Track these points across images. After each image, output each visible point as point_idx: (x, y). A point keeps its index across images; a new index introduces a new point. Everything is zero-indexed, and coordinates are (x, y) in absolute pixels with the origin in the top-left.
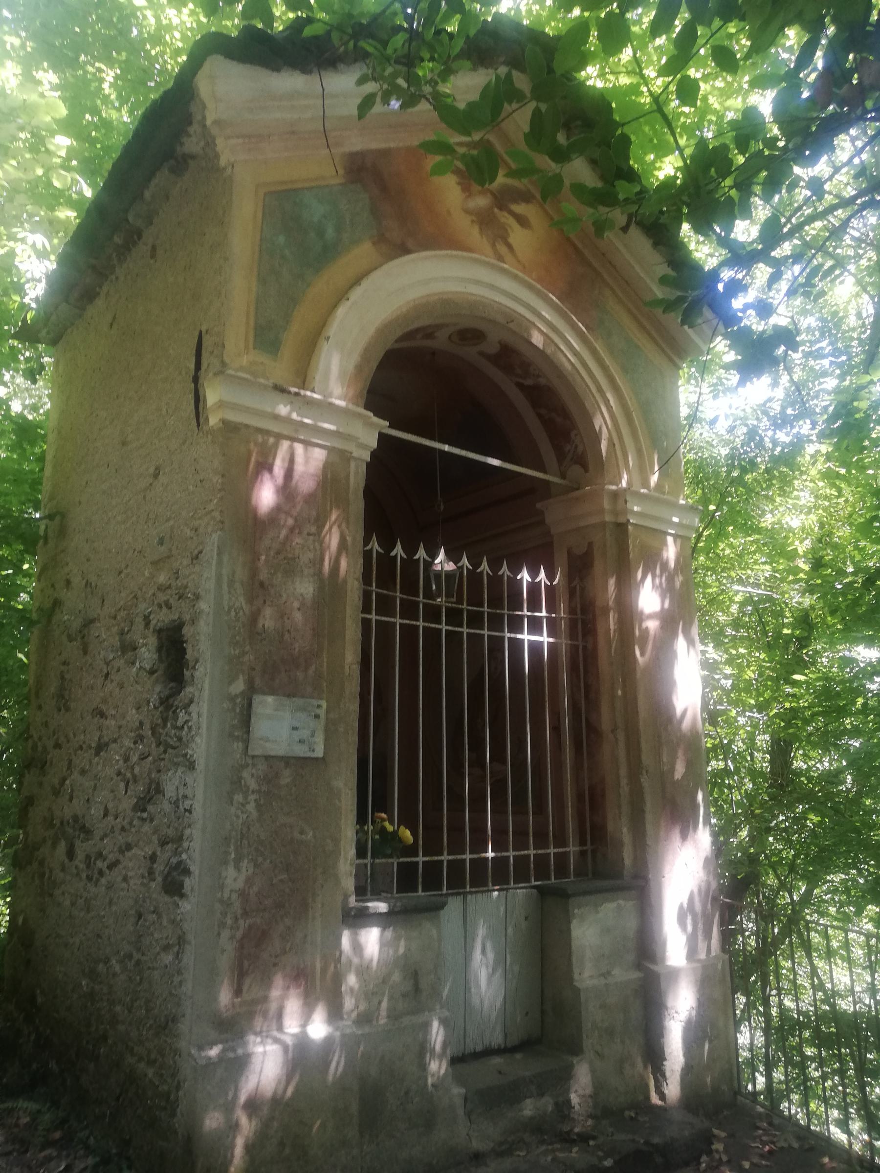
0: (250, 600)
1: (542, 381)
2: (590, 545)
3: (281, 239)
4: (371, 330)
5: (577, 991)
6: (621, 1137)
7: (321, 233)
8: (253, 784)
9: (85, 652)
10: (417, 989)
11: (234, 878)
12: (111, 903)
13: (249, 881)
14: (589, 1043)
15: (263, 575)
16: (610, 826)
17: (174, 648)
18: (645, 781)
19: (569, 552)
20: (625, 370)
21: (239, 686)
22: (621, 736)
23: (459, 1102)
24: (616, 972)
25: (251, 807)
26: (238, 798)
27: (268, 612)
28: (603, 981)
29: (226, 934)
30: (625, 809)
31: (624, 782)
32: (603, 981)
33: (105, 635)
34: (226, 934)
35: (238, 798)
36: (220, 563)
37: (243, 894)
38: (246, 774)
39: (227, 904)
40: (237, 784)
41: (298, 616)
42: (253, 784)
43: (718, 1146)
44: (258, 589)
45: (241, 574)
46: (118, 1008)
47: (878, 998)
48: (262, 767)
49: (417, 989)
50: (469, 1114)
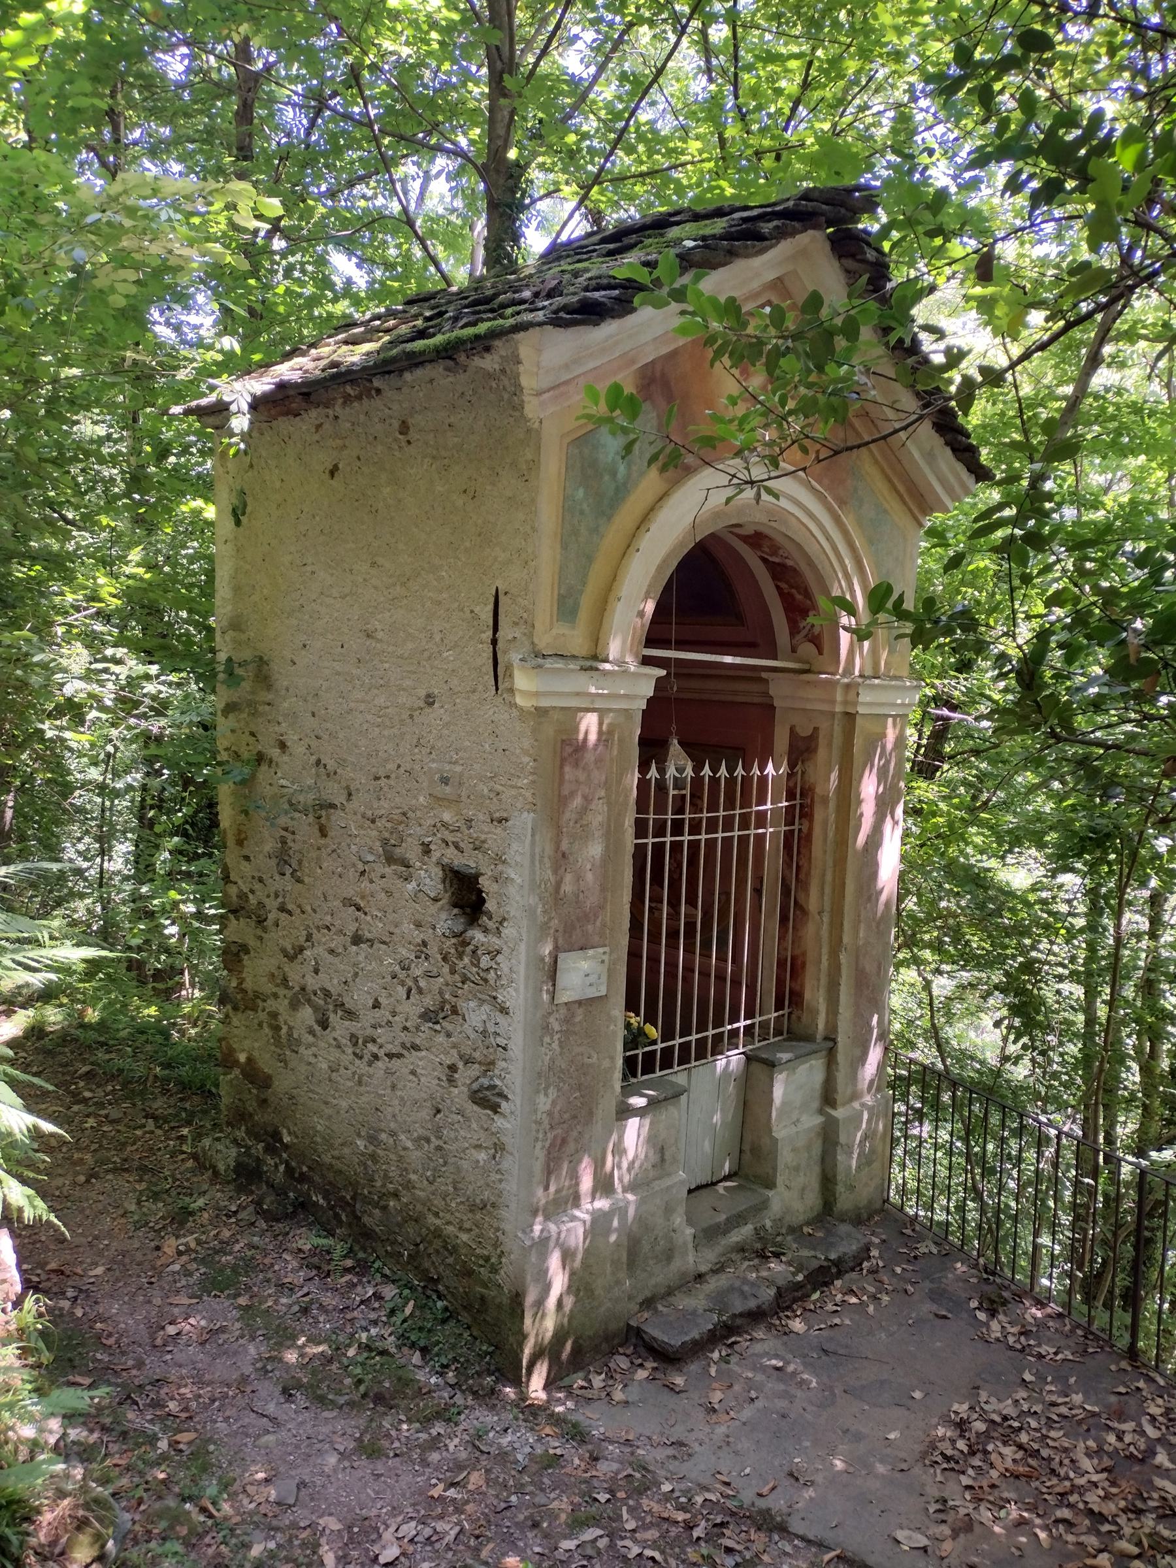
0: (555, 872)
1: (790, 563)
2: (816, 729)
3: (581, 493)
4: (653, 570)
5: (775, 1141)
6: (806, 1253)
7: (614, 474)
8: (557, 1027)
9: (323, 832)
10: (663, 1160)
11: (544, 1103)
12: (393, 1087)
13: (554, 1103)
14: (780, 1180)
15: (564, 846)
16: (807, 995)
17: (467, 896)
18: (843, 958)
19: (792, 729)
20: (871, 541)
21: (547, 949)
22: (826, 919)
23: (690, 1239)
24: (804, 1118)
25: (555, 1046)
26: (547, 1039)
27: (568, 878)
28: (794, 1129)
29: (539, 1145)
30: (824, 980)
31: (825, 958)
32: (794, 1129)
33: (357, 838)
34: (539, 1145)
35: (547, 1039)
36: (533, 843)
37: (550, 1114)
38: (552, 1020)
39: (539, 1123)
40: (546, 1028)
41: (590, 877)
42: (557, 1027)
43: (875, 1253)
44: (561, 859)
45: (549, 849)
46: (413, 1177)
47: (1137, 1563)
48: (563, 1011)
49: (663, 1160)
50: (696, 1248)
